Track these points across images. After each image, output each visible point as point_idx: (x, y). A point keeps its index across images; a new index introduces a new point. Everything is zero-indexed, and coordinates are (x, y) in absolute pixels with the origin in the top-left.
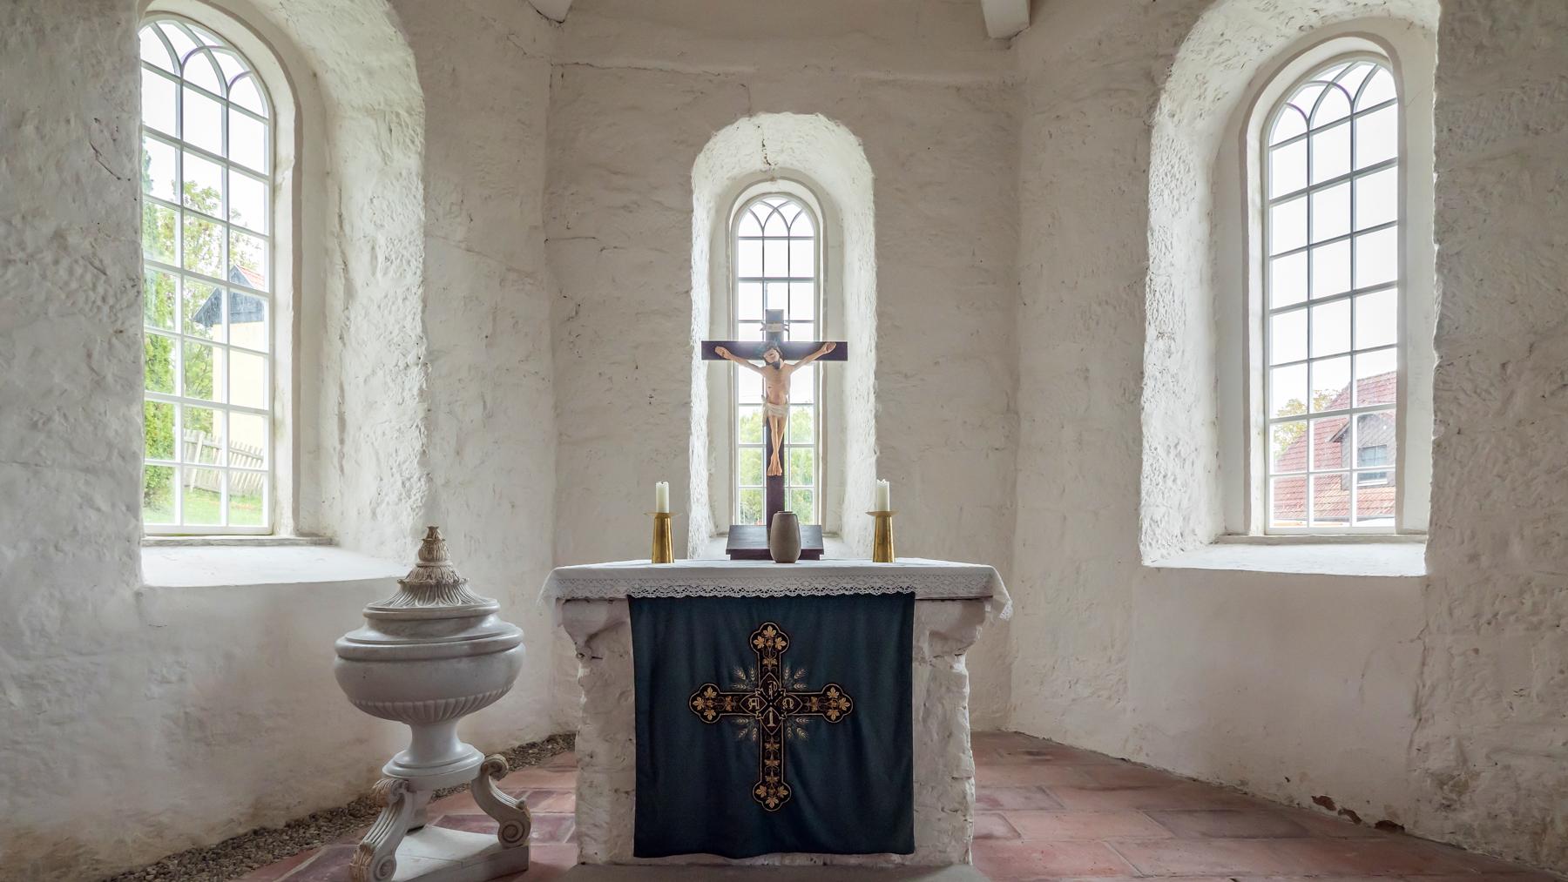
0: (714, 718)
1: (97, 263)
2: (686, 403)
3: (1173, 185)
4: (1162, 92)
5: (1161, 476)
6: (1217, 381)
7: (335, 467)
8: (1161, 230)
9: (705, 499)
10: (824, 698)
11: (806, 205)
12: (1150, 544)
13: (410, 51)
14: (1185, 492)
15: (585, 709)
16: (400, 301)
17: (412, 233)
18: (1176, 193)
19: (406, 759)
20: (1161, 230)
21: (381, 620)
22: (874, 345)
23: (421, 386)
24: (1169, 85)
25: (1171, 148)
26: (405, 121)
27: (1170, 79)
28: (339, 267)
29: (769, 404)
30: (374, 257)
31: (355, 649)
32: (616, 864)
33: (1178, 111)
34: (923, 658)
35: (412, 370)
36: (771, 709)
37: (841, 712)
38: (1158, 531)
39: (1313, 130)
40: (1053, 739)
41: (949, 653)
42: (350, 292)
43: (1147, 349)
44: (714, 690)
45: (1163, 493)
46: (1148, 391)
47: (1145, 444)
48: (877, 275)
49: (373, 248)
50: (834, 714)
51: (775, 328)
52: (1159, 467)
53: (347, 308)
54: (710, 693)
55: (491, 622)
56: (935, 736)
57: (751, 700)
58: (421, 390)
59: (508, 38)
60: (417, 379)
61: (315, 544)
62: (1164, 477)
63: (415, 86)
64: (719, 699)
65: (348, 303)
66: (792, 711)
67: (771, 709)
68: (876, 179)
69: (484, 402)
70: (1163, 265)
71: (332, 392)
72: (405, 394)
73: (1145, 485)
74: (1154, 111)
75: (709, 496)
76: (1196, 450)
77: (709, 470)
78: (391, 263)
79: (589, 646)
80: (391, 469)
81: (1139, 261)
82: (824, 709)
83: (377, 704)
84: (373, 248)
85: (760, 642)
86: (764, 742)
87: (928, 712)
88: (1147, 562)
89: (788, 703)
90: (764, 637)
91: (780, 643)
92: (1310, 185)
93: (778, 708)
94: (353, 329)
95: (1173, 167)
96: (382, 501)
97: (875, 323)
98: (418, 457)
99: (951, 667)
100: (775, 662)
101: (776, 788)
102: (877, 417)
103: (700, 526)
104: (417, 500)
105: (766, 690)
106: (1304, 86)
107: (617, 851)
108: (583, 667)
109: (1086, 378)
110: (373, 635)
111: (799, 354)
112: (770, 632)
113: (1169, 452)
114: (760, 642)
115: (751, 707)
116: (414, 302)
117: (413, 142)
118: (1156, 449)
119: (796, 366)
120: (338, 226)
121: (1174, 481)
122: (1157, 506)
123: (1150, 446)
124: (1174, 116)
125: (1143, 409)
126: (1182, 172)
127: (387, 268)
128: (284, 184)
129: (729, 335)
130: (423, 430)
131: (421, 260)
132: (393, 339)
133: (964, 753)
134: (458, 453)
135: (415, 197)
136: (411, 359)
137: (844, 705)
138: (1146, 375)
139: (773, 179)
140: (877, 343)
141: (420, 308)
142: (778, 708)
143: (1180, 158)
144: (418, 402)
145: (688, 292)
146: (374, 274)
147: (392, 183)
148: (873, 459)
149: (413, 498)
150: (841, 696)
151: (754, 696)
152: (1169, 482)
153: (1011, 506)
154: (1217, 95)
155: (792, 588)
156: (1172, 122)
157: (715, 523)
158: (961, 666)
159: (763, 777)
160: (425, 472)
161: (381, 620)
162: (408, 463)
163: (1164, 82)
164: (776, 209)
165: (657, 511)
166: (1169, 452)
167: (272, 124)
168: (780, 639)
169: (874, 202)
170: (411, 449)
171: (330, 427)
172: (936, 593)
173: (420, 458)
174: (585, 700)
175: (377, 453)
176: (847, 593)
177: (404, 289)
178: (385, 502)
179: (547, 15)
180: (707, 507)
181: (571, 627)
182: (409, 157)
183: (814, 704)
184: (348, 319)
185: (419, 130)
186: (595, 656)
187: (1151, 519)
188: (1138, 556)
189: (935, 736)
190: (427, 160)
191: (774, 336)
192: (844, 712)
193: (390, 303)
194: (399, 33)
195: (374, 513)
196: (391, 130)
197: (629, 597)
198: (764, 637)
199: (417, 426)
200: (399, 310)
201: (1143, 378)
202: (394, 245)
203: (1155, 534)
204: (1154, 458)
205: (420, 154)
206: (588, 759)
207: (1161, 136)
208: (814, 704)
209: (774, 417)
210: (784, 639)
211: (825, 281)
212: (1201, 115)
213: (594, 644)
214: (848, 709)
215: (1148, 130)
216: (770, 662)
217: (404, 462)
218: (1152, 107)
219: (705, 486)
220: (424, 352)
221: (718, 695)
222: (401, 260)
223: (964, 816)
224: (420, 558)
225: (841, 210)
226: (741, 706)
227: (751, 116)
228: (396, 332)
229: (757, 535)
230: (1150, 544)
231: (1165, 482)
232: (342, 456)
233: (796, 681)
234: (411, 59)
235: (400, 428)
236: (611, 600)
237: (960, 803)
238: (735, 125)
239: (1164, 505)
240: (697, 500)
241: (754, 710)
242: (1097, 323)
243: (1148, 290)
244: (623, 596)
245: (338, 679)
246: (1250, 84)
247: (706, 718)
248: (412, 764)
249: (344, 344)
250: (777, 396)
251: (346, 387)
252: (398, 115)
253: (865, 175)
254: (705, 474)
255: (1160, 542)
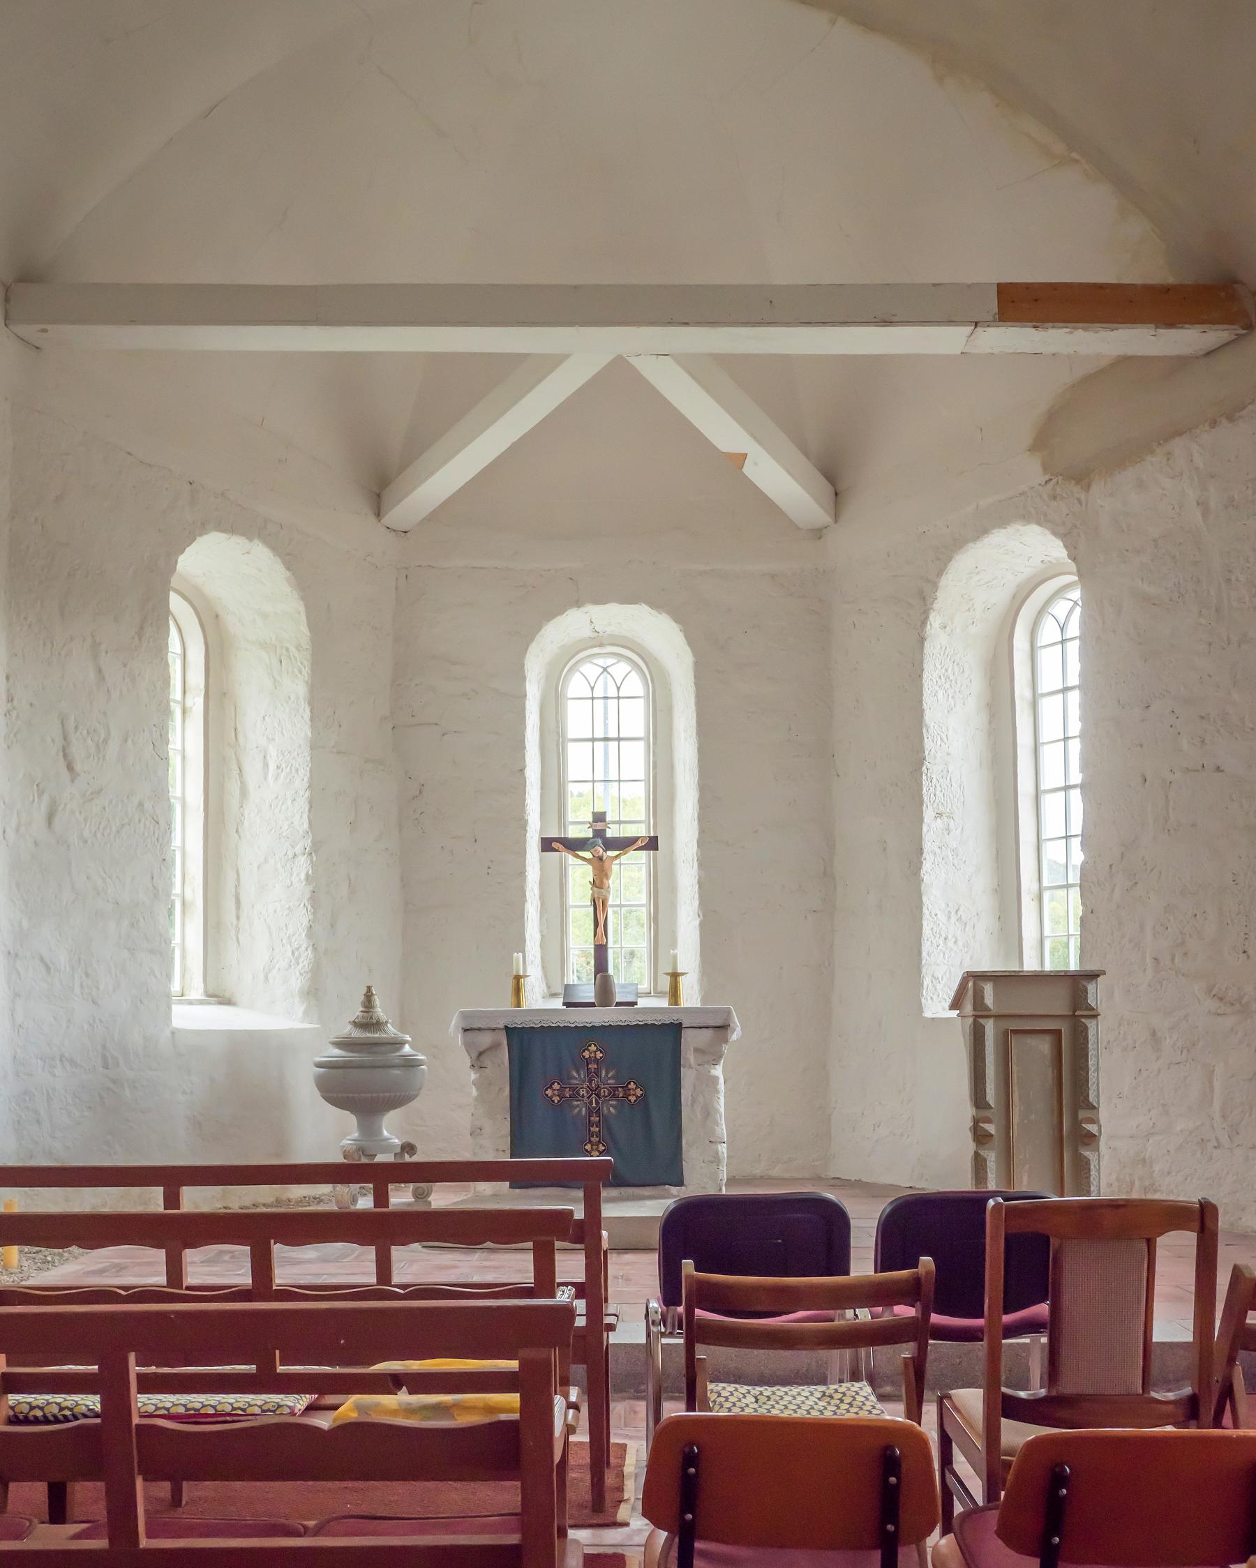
0: (559, 1101)
1: (155, 817)
2: (521, 873)
3: (948, 685)
4: (932, 611)
5: (942, 938)
6: (998, 852)
7: (232, 939)
8: (936, 726)
9: (538, 961)
10: (626, 1089)
11: (635, 665)
12: (932, 998)
13: (302, 603)
14: (966, 952)
15: (476, 1099)
16: (289, 802)
17: (300, 746)
18: (950, 692)
19: (356, 1135)
20: (936, 726)
21: (344, 1044)
22: (696, 815)
23: (307, 872)
24: (935, 606)
25: (944, 654)
26: (294, 657)
27: (936, 601)
28: (235, 773)
29: (595, 888)
30: (266, 765)
31: (330, 1061)
32: (496, 1195)
33: (950, 622)
34: (690, 1065)
35: (299, 858)
36: (594, 1095)
37: (637, 1097)
38: (939, 987)
39: (1066, 640)
40: (862, 1180)
41: (708, 1062)
42: (244, 793)
43: (925, 829)
44: (559, 1084)
45: (944, 954)
46: (928, 865)
47: (925, 910)
48: (698, 750)
49: (265, 757)
50: (633, 1099)
51: (599, 826)
52: (940, 931)
53: (242, 806)
54: (556, 1086)
55: (407, 1049)
56: (699, 1114)
57: (581, 1090)
58: (307, 876)
59: (365, 559)
60: (304, 866)
61: (221, 1003)
62: (945, 939)
63: (304, 629)
64: (562, 1089)
65: (243, 803)
66: (607, 1097)
67: (594, 1095)
68: (696, 662)
69: (350, 880)
70: (939, 755)
71: (230, 876)
72: (293, 878)
73: (926, 947)
74: (926, 626)
75: (541, 957)
76: (977, 914)
77: (541, 931)
78: (282, 770)
79: (479, 1059)
80: (282, 940)
81: (917, 752)
82: (626, 1096)
83: (349, 1095)
84: (265, 757)
85: (586, 1054)
86: (589, 1116)
87: (694, 1101)
88: (928, 1014)
89: (604, 1091)
90: (589, 1051)
91: (599, 1055)
92: (1065, 686)
93: (598, 1095)
94: (246, 824)
95: (946, 670)
96: (274, 968)
97: (697, 796)
98: (306, 931)
99: (709, 1072)
100: (596, 1066)
101: (597, 1145)
102: (700, 883)
103: (534, 987)
104: (304, 966)
105: (591, 1083)
106: (1058, 601)
107: (497, 1189)
108: (475, 1073)
109: (885, 849)
110: (337, 1052)
111: (624, 844)
112: (593, 1048)
113: (949, 917)
114: (586, 1054)
115: (581, 1094)
116: (302, 803)
117: (301, 673)
118: (936, 915)
119: (617, 857)
120: (234, 738)
121: (955, 942)
122: (938, 965)
123: (930, 913)
124: (945, 627)
125: (923, 880)
126: (956, 673)
127: (278, 774)
128: (193, 708)
129: (560, 833)
130: (309, 907)
131: (308, 769)
132: (282, 833)
133: (717, 1126)
134: (332, 926)
135: (302, 717)
136: (299, 849)
137: (639, 1092)
138: (925, 850)
139: (601, 645)
140: (699, 814)
141: (307, 809)
142: (598, 1095)
143: (954, 662)
144: (306, 885)
145: (522, 770)
146: (266, 778)
147: (282, 705)
148: (697, 922)
149: (301, 965)
150: (637, 1087)
151: (583, 1088)
152: (950, 944)
153: (829, 965)
154: (986, 606)
155: (606, 1021)
156: (945, 632)
157: (547, 984)
158: (718, 1071)
159: (589, 1138)
160: (311, 944)
161: (340, 1044)
162: (297, 935)
163: (932, 604)
164: (605, 669)
165: (514, 973)
166: (949, 917)
167: (183, 658)
168: (599, 1052)
169: (695, 683)
170: (299, 924)
171: (230, 905)
172: (695, 1023)
173: (307, 931)
174: (476, 1094)
175: (269, 928)
176: (640, 1023)
177: (293, 792)
178: (277, 968)
179: (394, 528)
180: (540, 968)
181: (468, 1046)
182: (297, 684)
183: (621, 1093)
184: (242, 815)
185: (306, 663)
186: (482, 1066)
187: (933, 976)
188: (920, 1008)
189: (699, 1114)
190: (313, 688)
191: (599, 834)
192: (639, 1097)
193: (281, 803)
194: (294, 592)
195: (266, 978)
196: (281, 662)
197: (506, 1027)
198: (589, 1051)
199: (305, 905)
200: (288, 809)
201: (922, 854)
202: (284, 756)
203: (936, 989)
204: (935, 923)
205: (307, 682)
206: (479, 1131)
207: (934, 646)
208: (621, 1093)
209: (599, 898)
210: (601, 1052)
211: (654, 744)
212: (973, 622)
213: (481, 1058)
214: (642, 1095)
215: (922, 640)
216: (593, 1066)
217: (294, 935)
218: (924, 623)
219: (538, 948)
220: (310, 844)
221: (561, 1087)
222: (291, 768)
223: (718, 1166)
224: (362, 1007)
225: (669, 675)
226: (575, 1094)
227: (579, 607)
228: (286, 827)
229: (588, 993)
230: (932, 998)
231: (945, 944)
232: (238, 930)
233: (609, 1079)
234: (302, 609)
235: (290, 907)
236: (494, 1030)
237: (715, 1157)
238: (565, 615)
239: (944, 964)
240: (532, 962)
241: (583, 1096)
242: (891, 801)
243: (924, 777)
244: (502, 1026)
245: (317, 1086)
246: (1014, 597)
247: (553, 1101)
248: (360, 1138)
249: (240, 837)
250: (602, 882)
251: (241, 872)
252: (287, 649)
253: (688, 658)
254: (538, 937)
255: (940, 996)
